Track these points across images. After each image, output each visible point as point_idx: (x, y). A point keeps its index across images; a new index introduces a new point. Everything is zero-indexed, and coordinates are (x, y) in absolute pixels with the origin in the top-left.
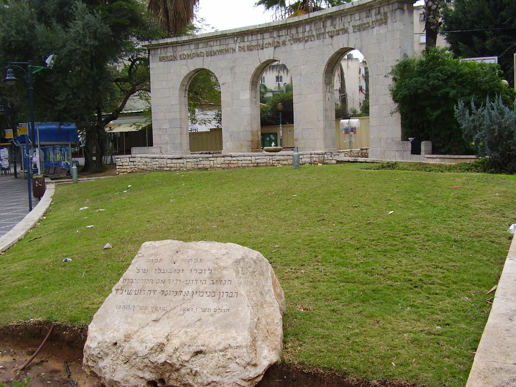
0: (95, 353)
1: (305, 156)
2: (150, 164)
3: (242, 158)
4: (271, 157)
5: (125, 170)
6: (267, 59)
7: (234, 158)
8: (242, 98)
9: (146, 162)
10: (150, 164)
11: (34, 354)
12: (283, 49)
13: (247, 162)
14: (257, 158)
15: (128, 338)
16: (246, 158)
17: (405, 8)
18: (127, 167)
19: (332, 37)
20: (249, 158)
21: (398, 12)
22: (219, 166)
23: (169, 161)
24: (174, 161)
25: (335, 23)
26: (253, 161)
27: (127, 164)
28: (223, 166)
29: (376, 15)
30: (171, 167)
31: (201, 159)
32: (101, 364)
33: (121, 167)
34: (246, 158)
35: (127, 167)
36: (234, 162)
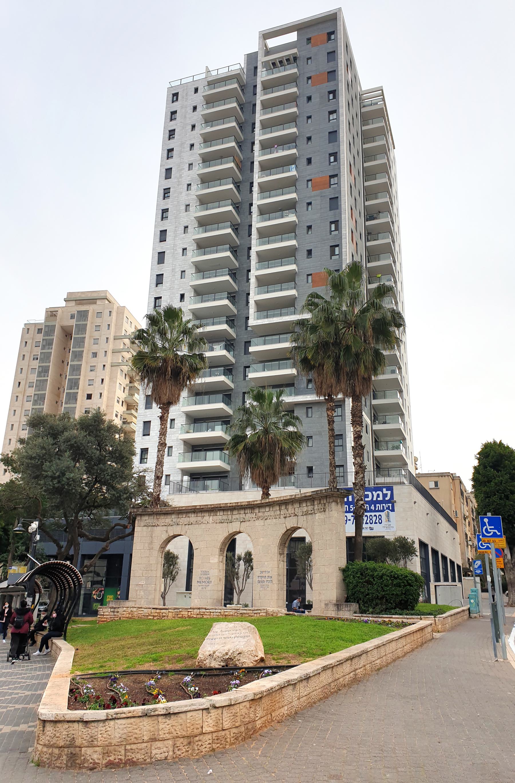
0: (203, 659)
1: (262, 611)
2: (136, 613)
3: (214, 611)
4: (236, 611)
5: (105, 619)
6: (235, 530)
7: (207, 611)
8: (211, 561)
9: (132, 611)
10: (136, 613)
11: (246, 608)
12: (247, 523)
13: (218, 614)
14: (225, 611)
15: (214, 653)
16: (217, 611)
17: (339, 501)
18: (107, 617)
19: (285, 517)
20: (219, 611)
21: (333, 504)
22: (195, 616)
23: (153, 611)
24: (158, 611)
25: (287, 507)
26: (222, 613)
27: (108, 613)
28: (199, 616)
29: (318, 504)
30: (154, 616)
31: (181, 610)
32: (205, 662)
33: (102, 616)
34: (217, 611)
35: (107, 617)
36: (207, 614)
